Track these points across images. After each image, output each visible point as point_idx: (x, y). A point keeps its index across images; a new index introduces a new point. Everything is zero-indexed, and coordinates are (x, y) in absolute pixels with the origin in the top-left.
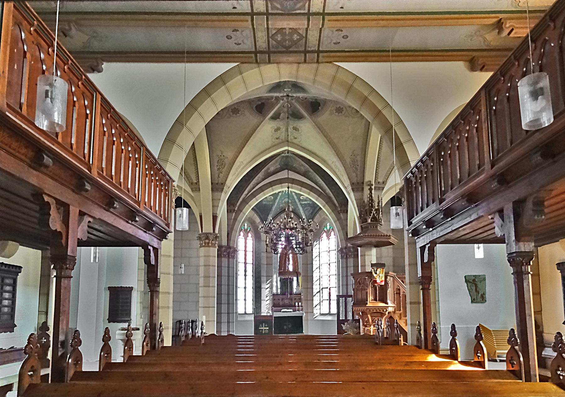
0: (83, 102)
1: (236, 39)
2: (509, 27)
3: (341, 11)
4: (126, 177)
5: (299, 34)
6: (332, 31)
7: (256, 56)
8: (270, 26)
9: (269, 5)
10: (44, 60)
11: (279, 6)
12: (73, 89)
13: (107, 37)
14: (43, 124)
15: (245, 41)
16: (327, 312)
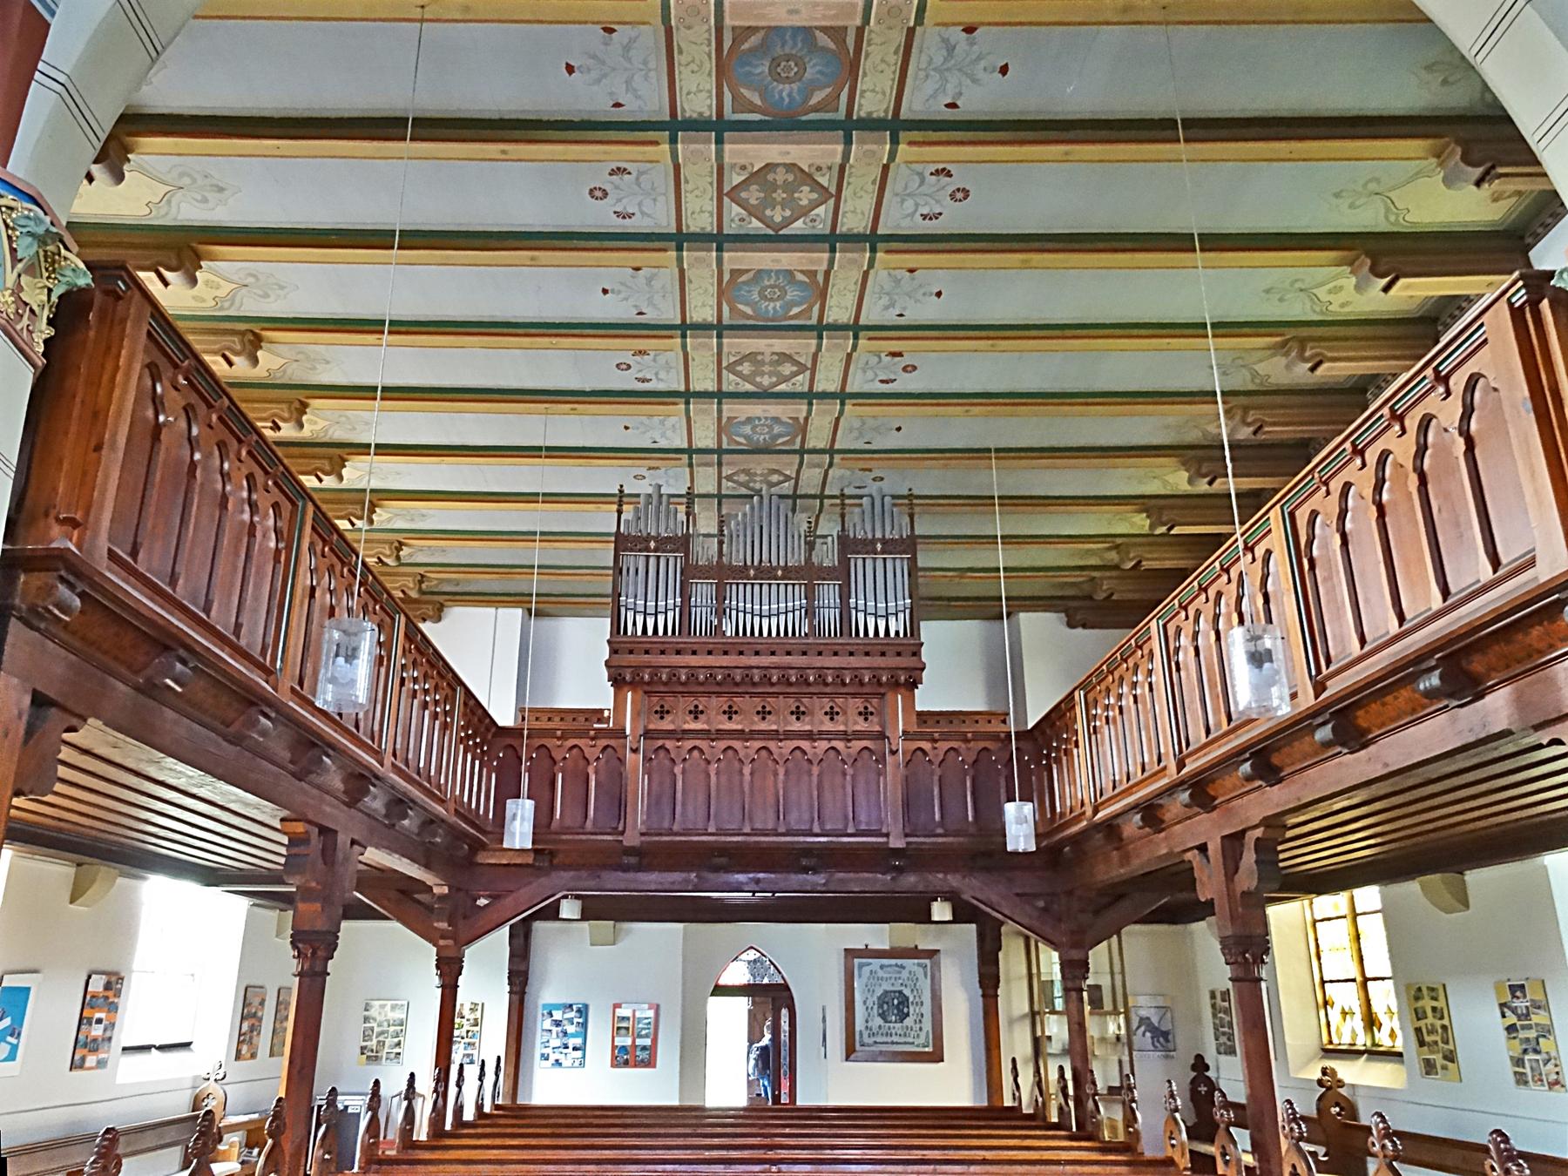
0: (218, 462)
1: (619, 200)
2: (1312, 357)
3: (950, 115)
4: (462, 790)
5: (817, 186)
6: (921, 175)
7: (690, 458)
8: (727, 160)
9: (728, 97)
10: (162, 397)
11: (749, 311)
12: (195, 431)
13: (282, 288)
14: (326, 698)
15: (662, 375)
16: (1358, 911)
